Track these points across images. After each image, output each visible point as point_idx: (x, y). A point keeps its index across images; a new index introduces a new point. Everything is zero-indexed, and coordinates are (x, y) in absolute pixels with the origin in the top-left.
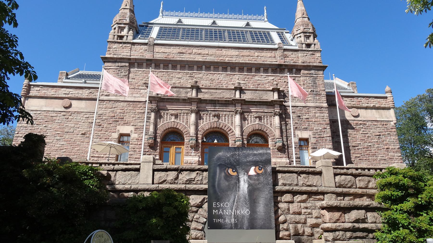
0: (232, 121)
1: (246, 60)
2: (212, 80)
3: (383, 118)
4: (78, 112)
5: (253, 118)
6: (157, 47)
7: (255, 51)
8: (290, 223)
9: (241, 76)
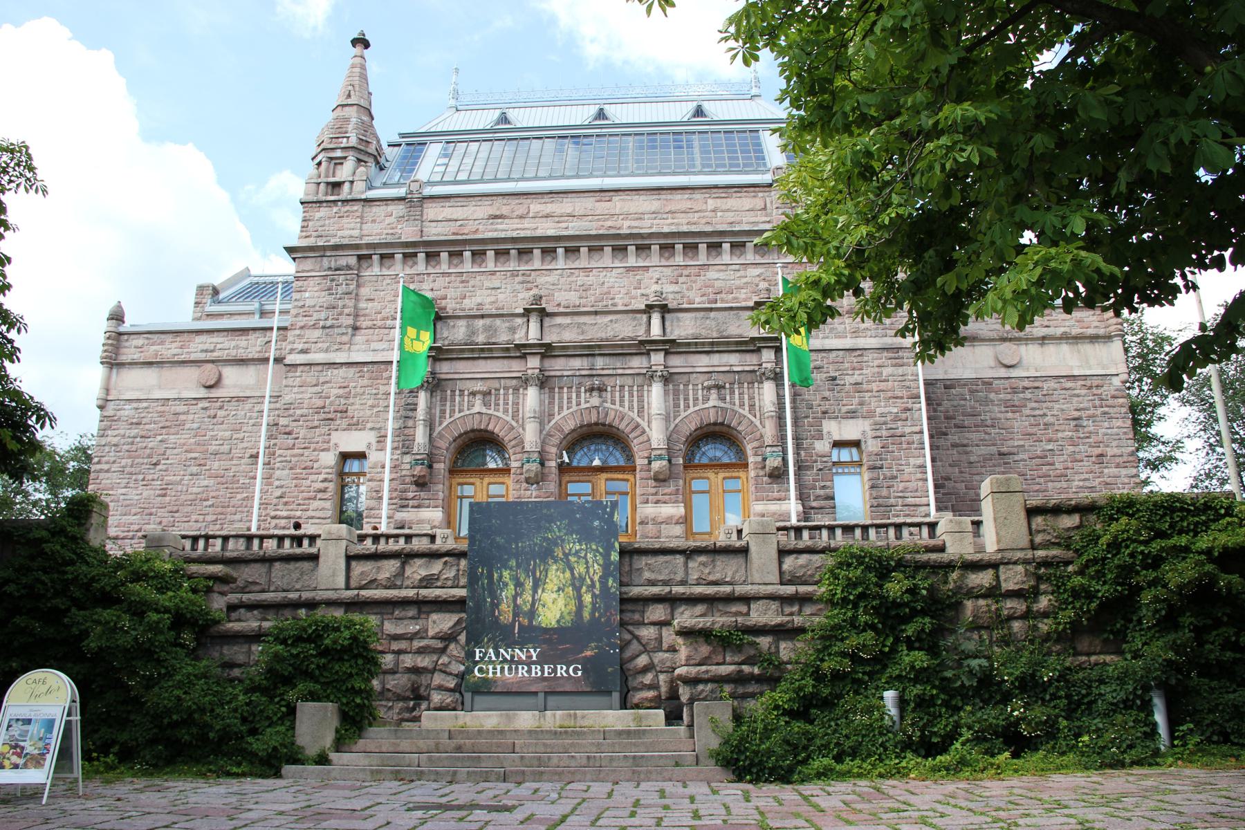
1: (682, 224)
3: (1090, 368)
4: (239, 399)
5: (700, 392)
7: (707, 195)
8: (661, 672)
9: (668, 271)
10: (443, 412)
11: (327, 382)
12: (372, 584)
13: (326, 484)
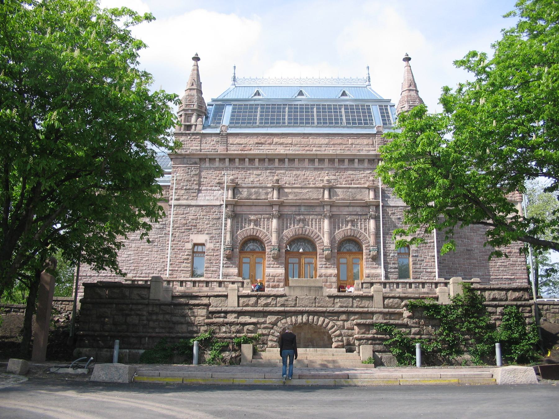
7: (349, 138)
10: (238, 227)
11: (187, 213)
12: (247, 305)
13: (188, 257)
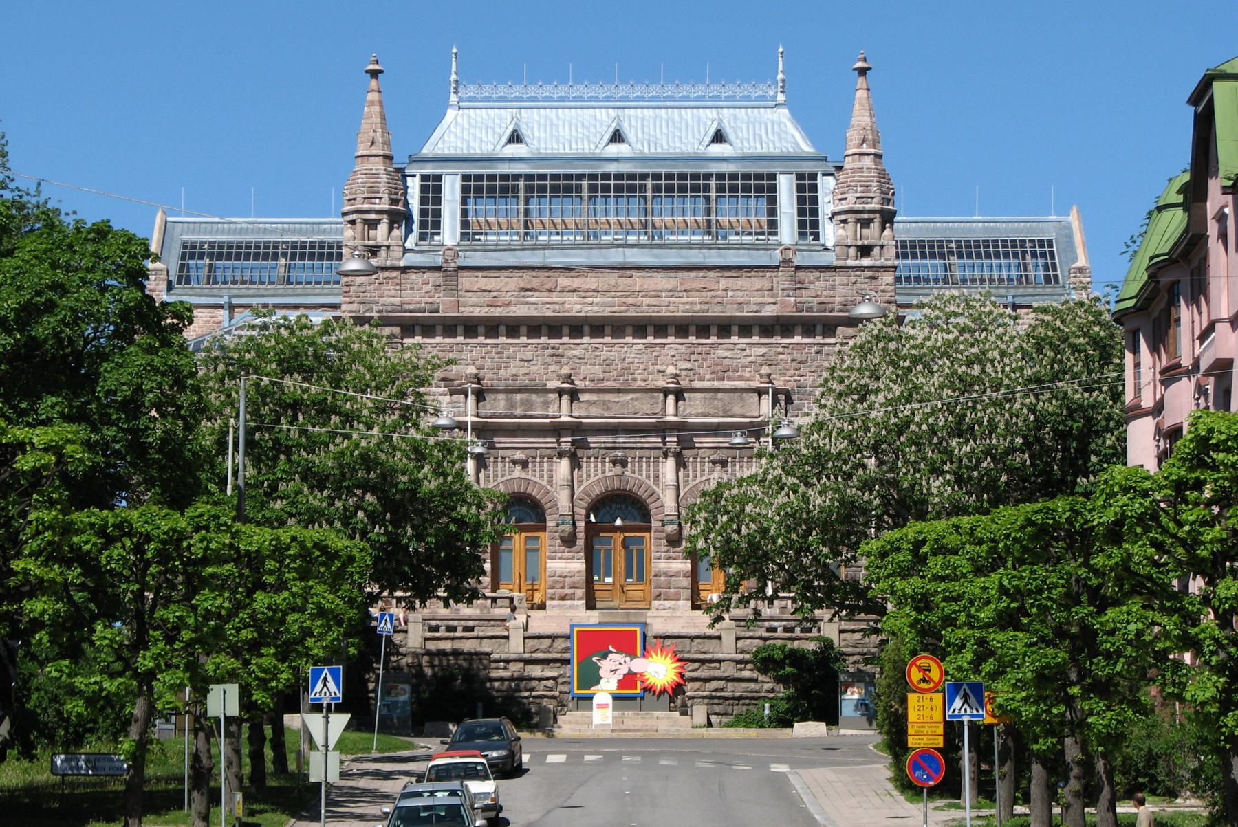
0: (656, 471)
2: (609, 362)
6: (465, 274)
7: (719, 274)
